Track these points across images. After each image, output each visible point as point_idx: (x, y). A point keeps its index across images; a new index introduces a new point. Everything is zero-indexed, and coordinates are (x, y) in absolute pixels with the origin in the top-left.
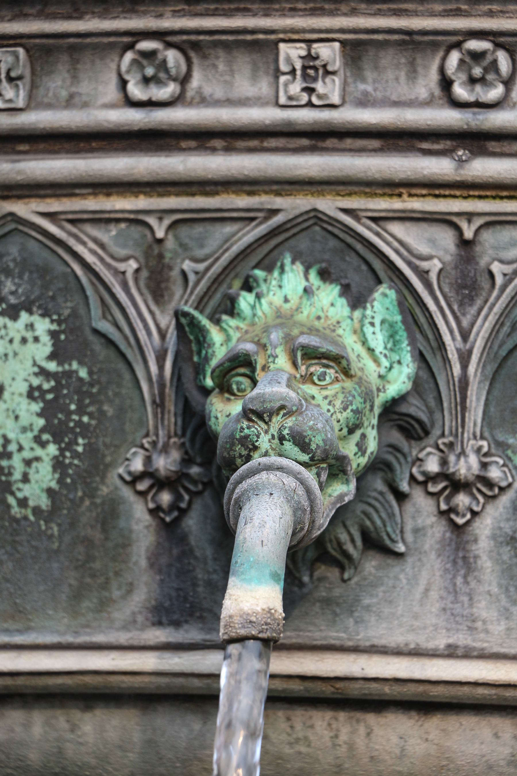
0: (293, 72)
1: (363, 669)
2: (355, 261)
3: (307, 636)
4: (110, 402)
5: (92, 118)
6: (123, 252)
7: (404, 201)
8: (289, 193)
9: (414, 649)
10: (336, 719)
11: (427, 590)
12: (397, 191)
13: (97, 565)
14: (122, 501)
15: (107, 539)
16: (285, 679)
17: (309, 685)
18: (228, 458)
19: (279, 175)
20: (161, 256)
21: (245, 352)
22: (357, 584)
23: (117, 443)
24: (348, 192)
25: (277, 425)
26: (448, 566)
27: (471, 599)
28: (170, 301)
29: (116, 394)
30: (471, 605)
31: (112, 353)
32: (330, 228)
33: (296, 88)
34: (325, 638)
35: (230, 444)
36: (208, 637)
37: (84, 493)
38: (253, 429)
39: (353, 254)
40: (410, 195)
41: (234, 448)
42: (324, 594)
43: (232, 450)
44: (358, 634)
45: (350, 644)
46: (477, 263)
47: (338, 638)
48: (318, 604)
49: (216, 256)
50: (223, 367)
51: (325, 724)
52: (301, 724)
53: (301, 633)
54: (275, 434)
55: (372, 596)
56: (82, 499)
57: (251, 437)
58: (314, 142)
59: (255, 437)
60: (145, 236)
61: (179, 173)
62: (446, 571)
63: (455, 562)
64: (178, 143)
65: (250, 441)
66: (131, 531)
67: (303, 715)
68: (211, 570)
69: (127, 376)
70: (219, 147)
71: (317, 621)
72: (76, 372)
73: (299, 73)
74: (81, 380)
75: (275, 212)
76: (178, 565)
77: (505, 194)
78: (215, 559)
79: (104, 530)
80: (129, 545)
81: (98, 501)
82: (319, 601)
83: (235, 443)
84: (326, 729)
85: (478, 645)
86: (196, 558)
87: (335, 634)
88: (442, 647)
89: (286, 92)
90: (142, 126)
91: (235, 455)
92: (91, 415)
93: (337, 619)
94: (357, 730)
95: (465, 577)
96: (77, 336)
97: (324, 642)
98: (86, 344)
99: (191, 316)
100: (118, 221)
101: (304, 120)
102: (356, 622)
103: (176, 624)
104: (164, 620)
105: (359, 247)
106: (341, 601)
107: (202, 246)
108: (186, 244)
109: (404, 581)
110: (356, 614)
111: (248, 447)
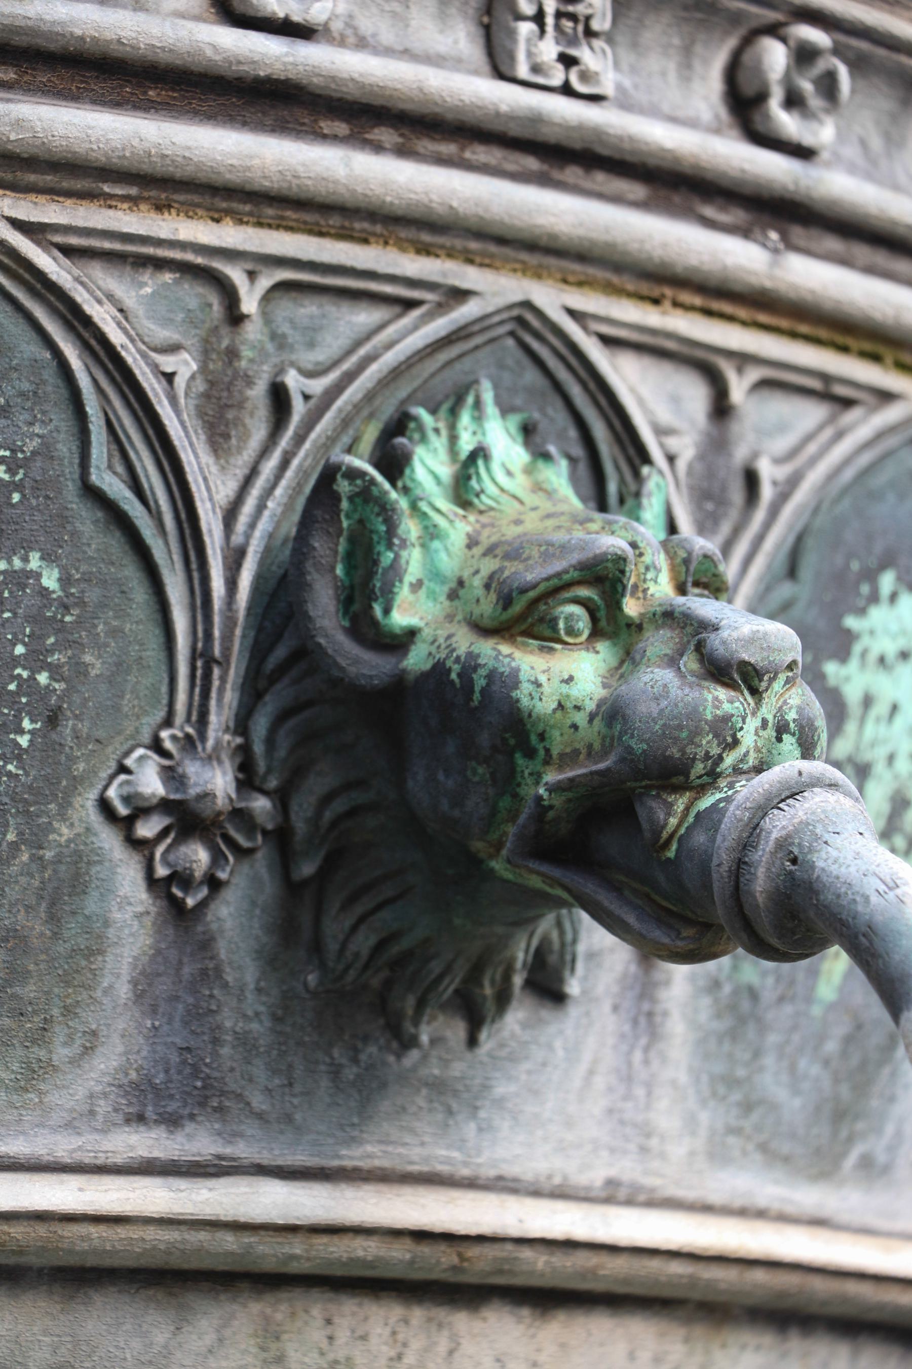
0: (539, 18)
1: (521, 1221)
2: (561, 417)
3: (399, 1155)
4: (100, 647)
5: (183, 33)
6: (164, 335)
7: (664, 313)
8: (487, 261)
9: (560, 1186)
10: (406, 1322)
11: (591, 1072)
12: (656, 292)
13: (29, 991)
14: (99, 857)
15: (56, 936)
16: (388, 1239)
17: (426, 1250)
18: (679, 759)
19: (507, 220)
20: (232, 354)
21: (619, 553)
22: (490, 1055)
23: (100, 734)
24: (582, 278)
25: (774, 700)
26: (627, 1028)
27: (649, 1094)
28: (239, 450)
29: (114, 632)
30: (648, 1107)
31: (115, 543)
32: (535, 345)
33: (549, 50)
34: (426, 1160)
35: (691, 732)
36: (228, 1151)
37: (20, 834)
38: (737, 704)
39: (559, 403)
40: (676, 304)
41: (697, 740)
42: (436, 1072)
43: (693, 743)
44: (479, 1153)
45: (465, 1172)
46: (730, 455)
47: (448, 1161)
48: (424, 1091)
49: (346, 366)
50: (560, 579)
51: (387, 1331)
52: (348, 1334)
53: (390, 1149)
54: (770, 718)
55: (510, 1078)
56: (14, 847)
57: (734, 719)
58: (545, 167)
59: (740, 719)
60: (210, 305)
61: (336, 182)
62: (623, 1036)
63: (635, 1022)
64: (316, 121)
65: (731, 728)
66: (107, 924)
67: (353, 1314)
68: (250, 1013)
69: (140, 594)
70: (388, 146)
71: (417, 1124)
72: (38, 576)
73: (550, 21)
74: (44, 592)
75: (460, 295)
76: (191, 1000)
77: (804, 329)
78: (259, 990)
79: (53, 918)
80: (101, 952)
81: (49, 854)
82: (427, 1084)
83: (702, 729)
84: (386, 1343)
85: (650, 1181)
86: (225, 985)
87: (443, 1152)
88: (599, 1183)
89: (530, 54)
90: (278, 71)
91: (696, 754)
92: (55, 672)
93: (451, 1122)
94: (435, 1343)
95: (646, 1049)
96: (47, 497)
97: (425, 1168)
98: (63, 518)
99: (367, 478)
100: (160, 264)
101: (563, 118)
102: (480, 1130)
103: (172, 1122)
104: (150, 1112)
105: (576, 392)
106: (460, 1087)
107: (311, 345)
108: (284, 336)
109: (560, 1053)
110: (482, 1114)
111: (725, 740)
